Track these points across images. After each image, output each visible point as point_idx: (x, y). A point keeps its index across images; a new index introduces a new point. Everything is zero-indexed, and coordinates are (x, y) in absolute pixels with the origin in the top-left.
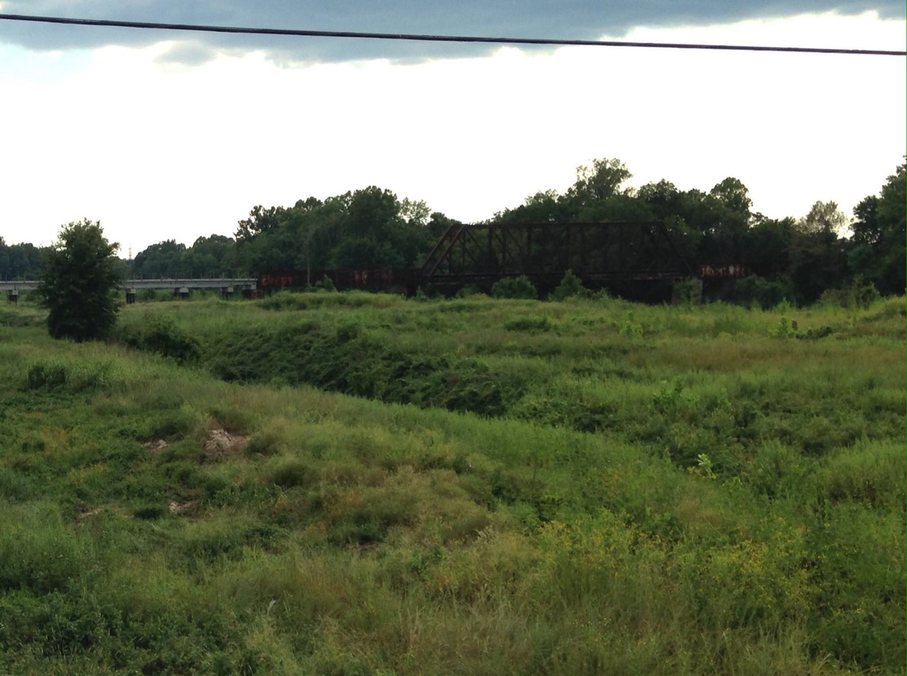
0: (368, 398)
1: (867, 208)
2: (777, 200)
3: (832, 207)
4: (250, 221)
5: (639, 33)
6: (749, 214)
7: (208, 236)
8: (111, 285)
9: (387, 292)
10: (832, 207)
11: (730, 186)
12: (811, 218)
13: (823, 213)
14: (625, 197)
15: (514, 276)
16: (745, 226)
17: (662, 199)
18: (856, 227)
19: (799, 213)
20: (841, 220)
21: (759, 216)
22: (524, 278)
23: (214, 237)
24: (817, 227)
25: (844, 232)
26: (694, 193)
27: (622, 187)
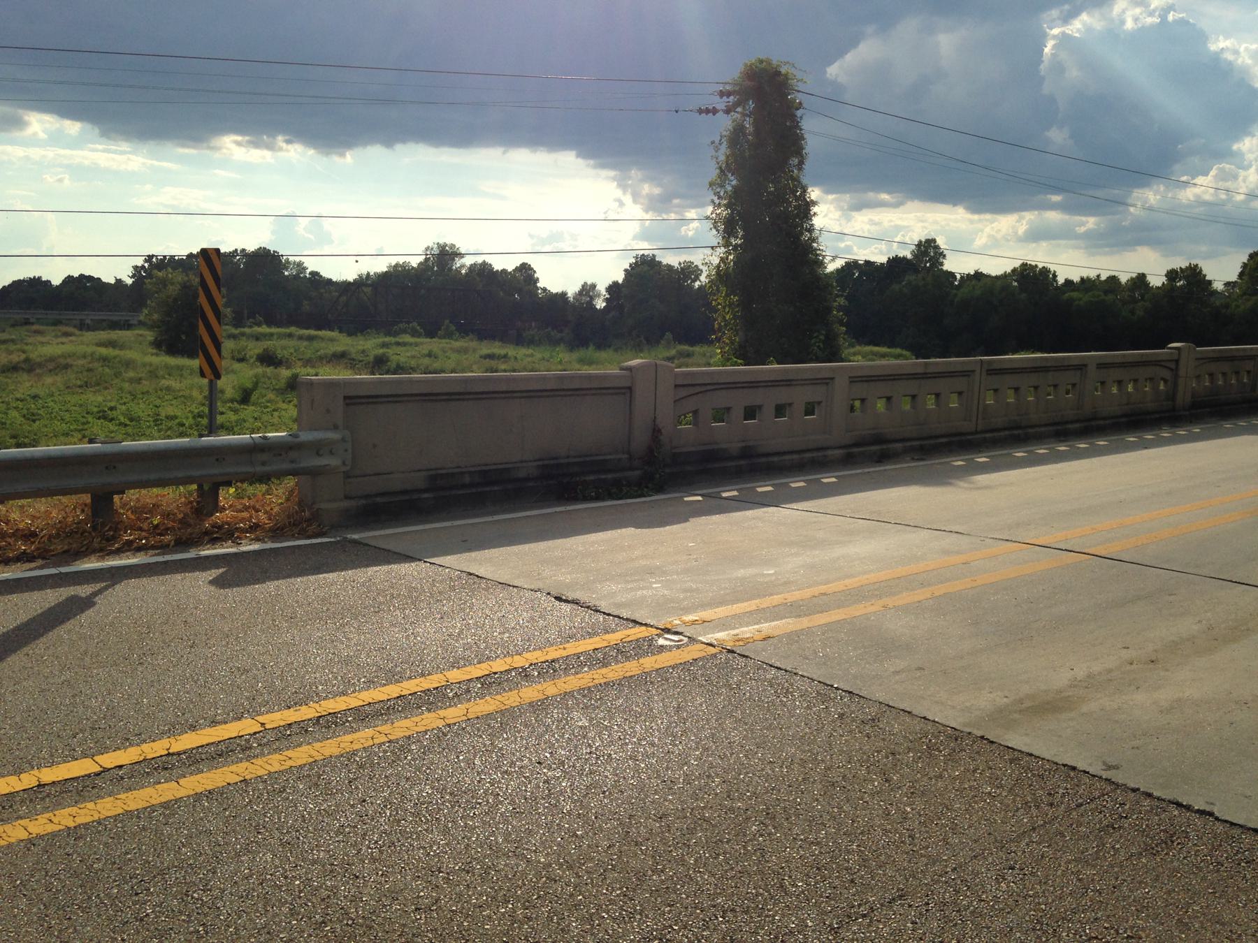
0: (615, 284)
1: (614, 288)
2: (557, 278)
3: (593, 286)
4: (143, 267)
5: (794, 506)
6: (537, 288)
7: (76, 275)
8: (592, 298)
9: (838, 270)
10: (593, 286)
11: (525, 269)
12: (581, 293)
13: (588, 291)
14: (458, 271)
15: (408, 323)
16: (537, 294)
17: (483, 272)
18: (607, 300)
19: (572, 290)
20: (599, 295)
21: (544, 290)
22: (415, 324)
23: (82, 276)
24: (585, 299)
25: (600, 304)
26: (504, 271)
27: (458, 263)
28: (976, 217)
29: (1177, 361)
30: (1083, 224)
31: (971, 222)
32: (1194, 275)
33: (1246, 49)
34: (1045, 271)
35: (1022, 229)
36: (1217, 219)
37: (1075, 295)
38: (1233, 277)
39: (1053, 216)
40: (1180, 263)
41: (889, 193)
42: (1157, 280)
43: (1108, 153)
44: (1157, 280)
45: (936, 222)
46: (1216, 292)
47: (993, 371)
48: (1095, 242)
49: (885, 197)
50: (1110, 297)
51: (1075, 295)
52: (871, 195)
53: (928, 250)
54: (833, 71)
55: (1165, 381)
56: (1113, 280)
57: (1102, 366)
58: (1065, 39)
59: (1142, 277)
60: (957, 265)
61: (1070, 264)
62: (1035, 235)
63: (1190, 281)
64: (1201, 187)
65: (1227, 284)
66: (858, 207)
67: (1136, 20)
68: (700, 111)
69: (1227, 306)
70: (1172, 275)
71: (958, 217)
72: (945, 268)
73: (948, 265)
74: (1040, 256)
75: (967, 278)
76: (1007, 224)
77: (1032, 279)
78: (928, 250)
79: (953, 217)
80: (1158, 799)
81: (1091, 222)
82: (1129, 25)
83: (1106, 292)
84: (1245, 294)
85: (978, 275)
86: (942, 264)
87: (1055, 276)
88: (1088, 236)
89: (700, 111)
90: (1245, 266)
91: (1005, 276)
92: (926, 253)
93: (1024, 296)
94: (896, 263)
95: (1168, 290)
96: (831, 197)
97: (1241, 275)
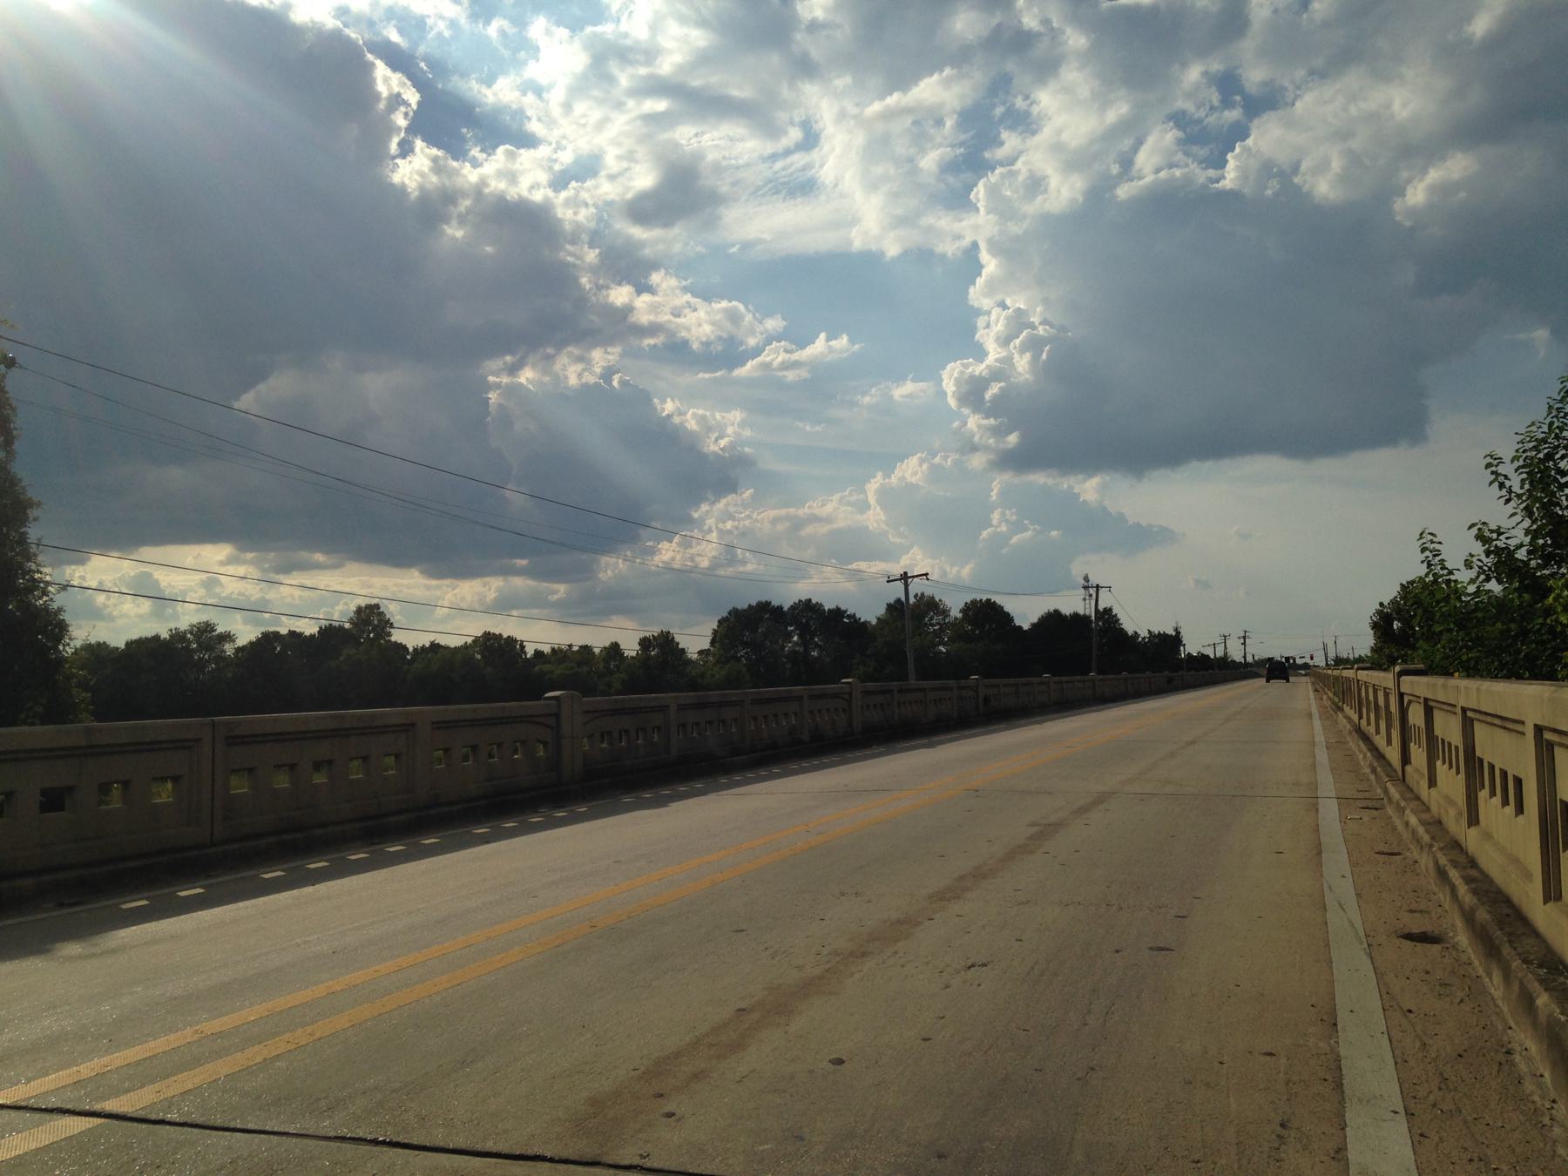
28: (434, 582)
29: (557, 716)
30: (556, 592)
31: (428, 588)
32: (665, 642)
33: (694, 414)
34: (511, 641)
35: (492, 595)
36: (683, 580)
37: (546, 667)
38: (706, 644)
39: (519, 583)
40: (653, 630)
41: (326, 553)
42: (631, 648)
43: (575, 516)
44: (631, 648)
45: (385, 588)
46: (690, 661)
47: (234, 740)
48: (568, 613)
49: (319, 557)
50: (585, 669)
51: (546, 667)
52: (303, 555)
53: (371, 619)
54: (246, 401)
55: (545, 744)
56: (586, 649)
57: (439, 725)
58: (513, 391)
59: (615, 647)
60: (410, 637)
61: (539, 634)
62: (503, 605)
63: (662, 648)
64: (668, 552)
65: (700, 652)
66: (287, 569)
67: (580, 375)
68: (1409, 937)
69: (703, 676)
70: (645, 643)
71: (412, 581)
72: (393, 639)
73: (397, 636)
74: (507, 627)
75: (420, 652)
76: (468, 590)
77: (497, 649)
78: (371, 619)
79: (405, 582)
80: (1015, 853)
81: (561, 590)
82: (573, 381)
83: (579, 664)
84: (718, 662)
85: (435, 647)
86: (389, 634)
87: (523, 647)
88: (559, 604)
89: (1409, 937)
90: (715, 632)
91: (466, 647)
92: (367, 622)
93: (489, 670)
94: (330, 633)
95: (643, 659)
96: (250, 556)
97: (713, 642)
